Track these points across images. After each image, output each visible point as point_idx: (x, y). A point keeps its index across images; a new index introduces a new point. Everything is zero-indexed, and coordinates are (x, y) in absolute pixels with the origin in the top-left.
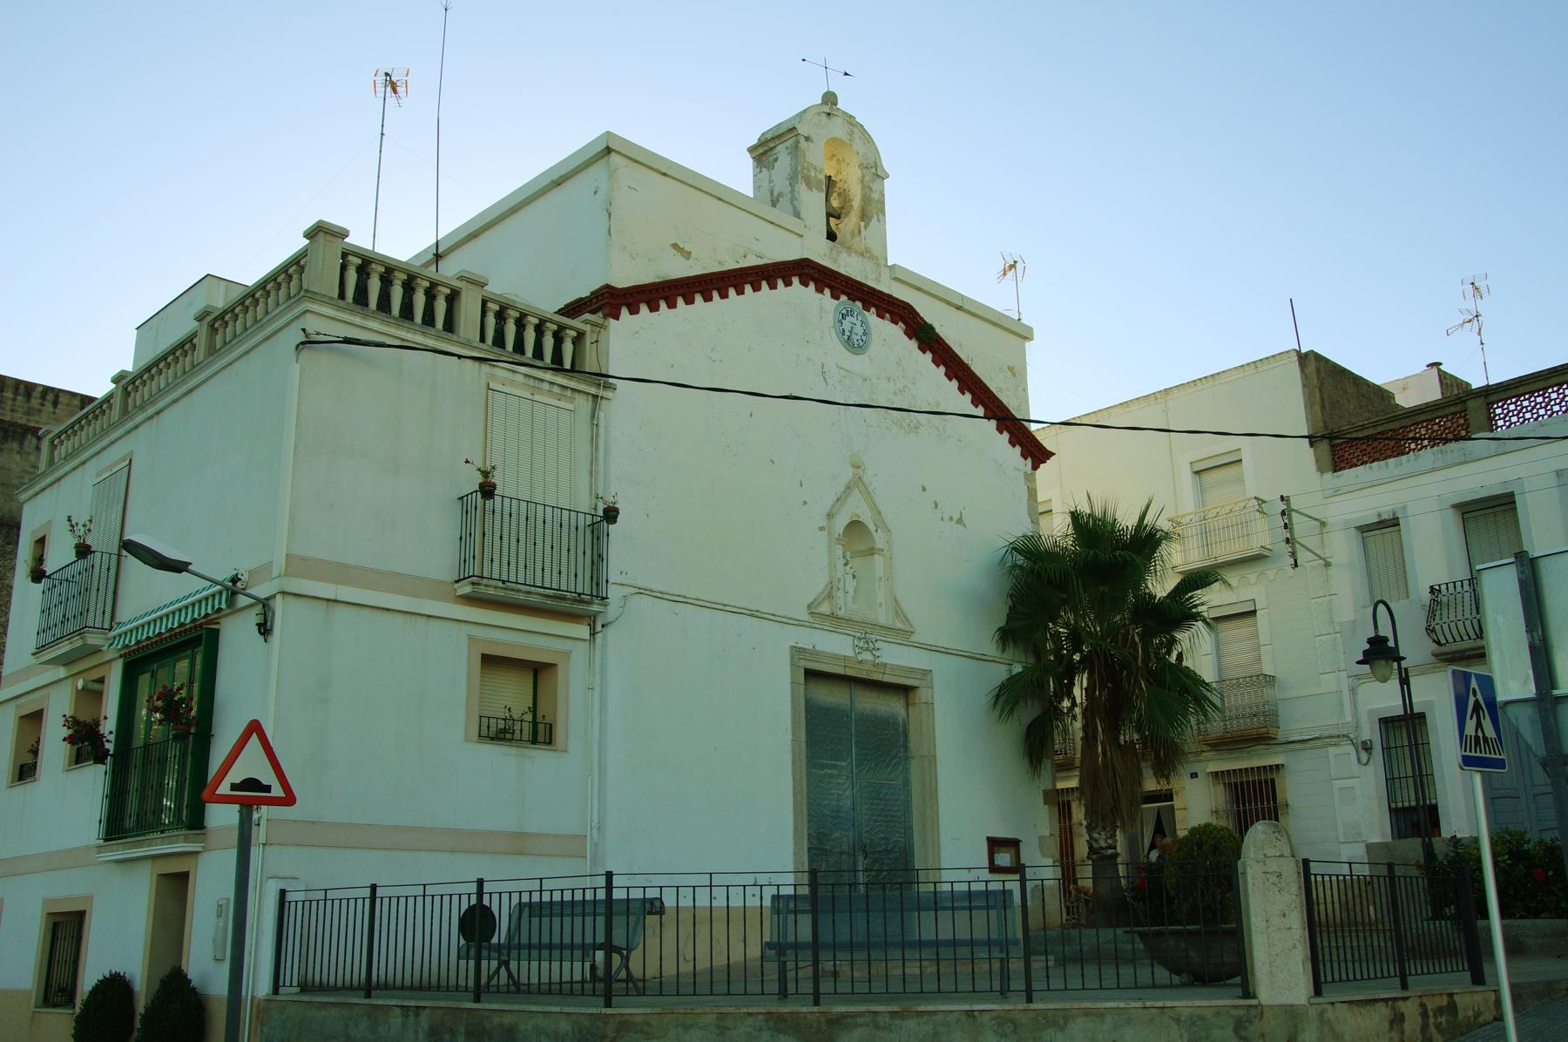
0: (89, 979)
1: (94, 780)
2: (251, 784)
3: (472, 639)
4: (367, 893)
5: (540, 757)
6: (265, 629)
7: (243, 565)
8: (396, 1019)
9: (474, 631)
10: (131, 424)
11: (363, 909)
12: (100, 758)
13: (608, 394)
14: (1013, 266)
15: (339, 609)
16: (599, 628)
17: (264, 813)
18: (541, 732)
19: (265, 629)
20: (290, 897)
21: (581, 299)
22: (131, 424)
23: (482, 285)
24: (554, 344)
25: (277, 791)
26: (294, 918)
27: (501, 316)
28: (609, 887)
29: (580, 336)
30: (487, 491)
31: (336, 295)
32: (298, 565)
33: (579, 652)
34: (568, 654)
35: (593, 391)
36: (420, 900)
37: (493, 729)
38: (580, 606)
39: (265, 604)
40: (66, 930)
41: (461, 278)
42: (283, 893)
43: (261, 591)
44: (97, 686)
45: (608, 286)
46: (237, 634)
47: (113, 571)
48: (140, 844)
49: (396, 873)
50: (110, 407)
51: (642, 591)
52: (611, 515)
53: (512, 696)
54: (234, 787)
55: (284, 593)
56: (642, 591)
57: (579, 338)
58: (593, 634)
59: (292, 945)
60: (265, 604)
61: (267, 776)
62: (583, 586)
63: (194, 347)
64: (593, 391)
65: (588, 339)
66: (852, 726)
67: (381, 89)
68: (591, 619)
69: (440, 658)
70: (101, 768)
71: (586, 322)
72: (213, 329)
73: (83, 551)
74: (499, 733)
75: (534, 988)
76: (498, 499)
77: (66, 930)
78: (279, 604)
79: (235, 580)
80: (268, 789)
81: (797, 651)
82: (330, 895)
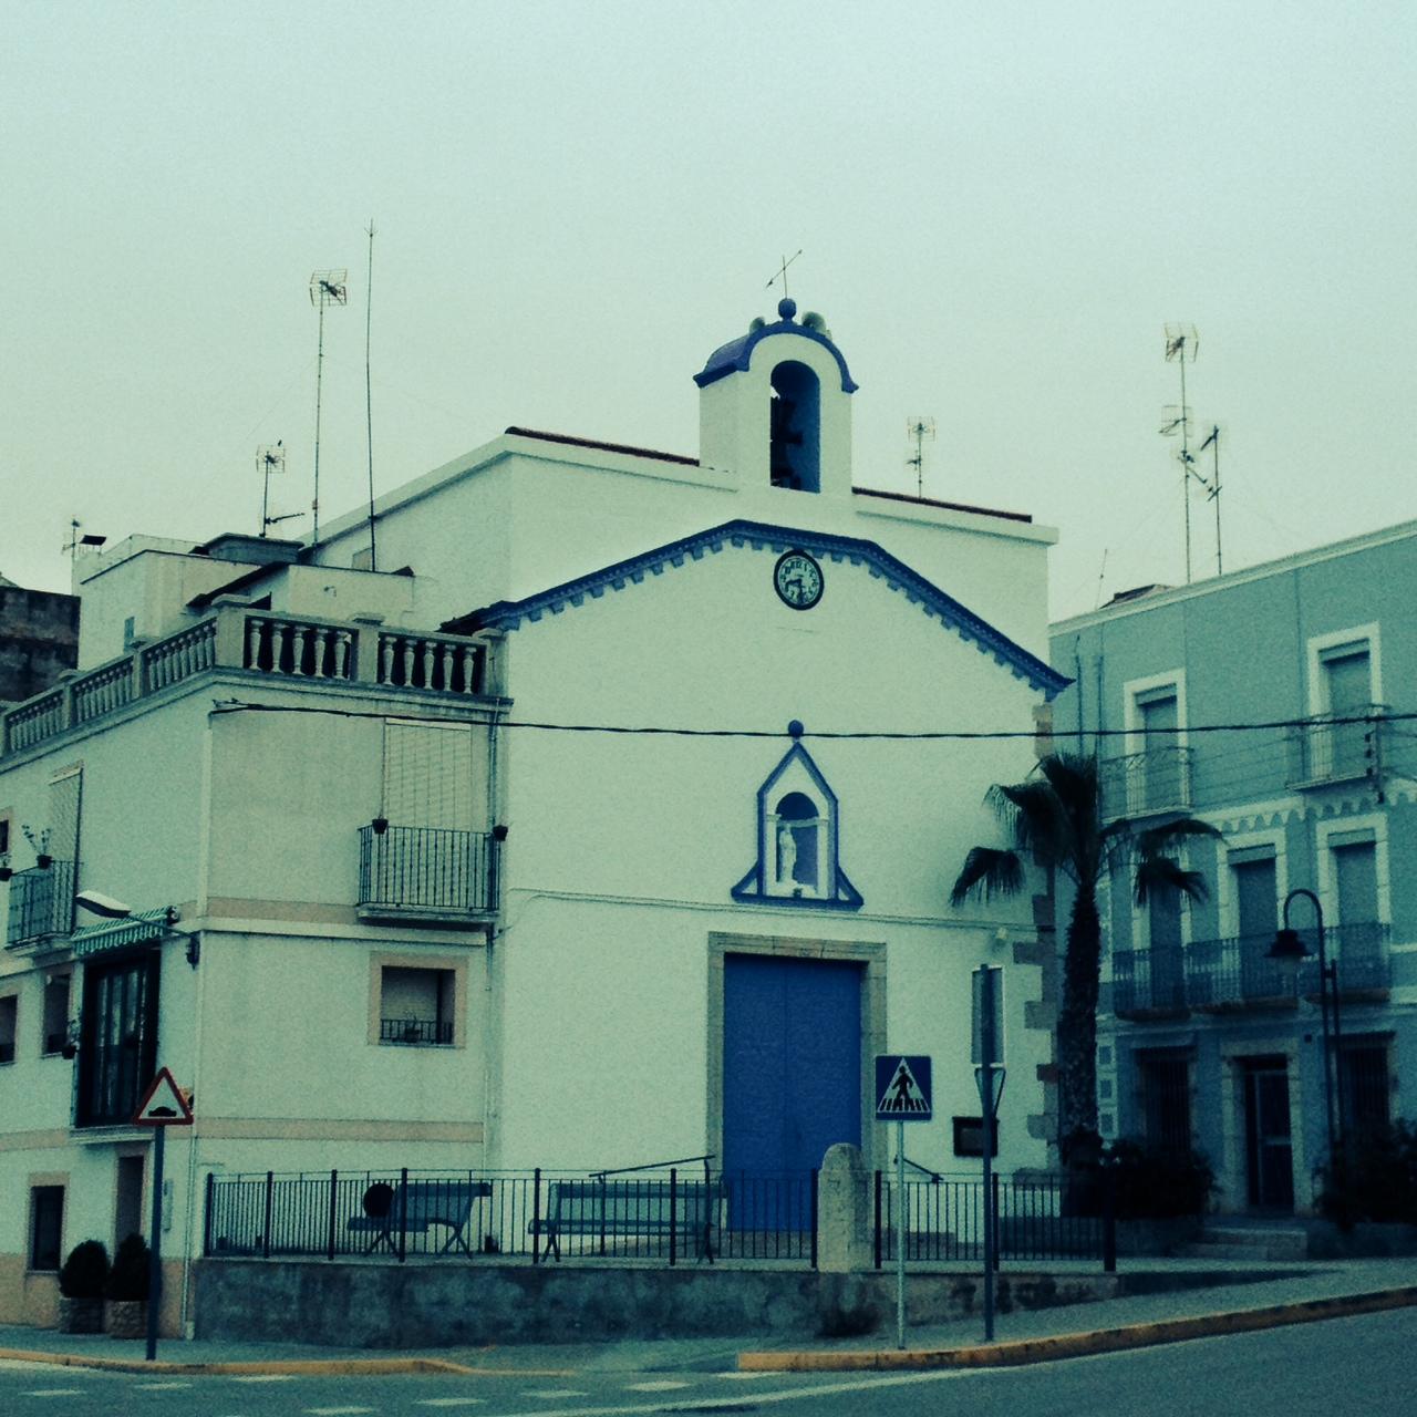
0: (70, 1244)
1: (63, 1073)
2: (163, 1111)
3: (373, 953)
4: (329, 1177)
5: (436, 1057)
6: (193, 958)
7: (175, 899)
8: (281, 1273)
9: (376, 947)
10: (79, 736)
11: (263, 1192)
12: (68, 1054)
13: (508, 708)
14: (1180, 343)
15: (255, 942)
16: (496, 934)
17: (170, 1130)
18: (443, 1034)
19: (193, 958)
20: (217, 1180)
21: (483, 609)
22: (79, 736)
23: (376, 623)
24: (454, 667)
25: (181, 1115)
26: (221, 1197)
27: (400, 647)
28: (404, 1178)
29: (481, 651)
30: (380, 825)
31: (240, 664)
32: (217, 905)
33: (477, 959)
34: (465, 959)
35: (490, 708)
36: (298, 1184)
37: (395, 1032)
38: (480, 922)
39: (193, 938)
40: (48, 1203)
41: (358, 620)
42: (210, 1177)
43: (186, 926)
44: (62, 981)
45: (502, 601)
46: (173, 959)
47: (71, 879)
48: (104, 1132)
49: (290, 1160)
50: (61, 701)
51: (540, 895)
52: (500, 833)
53: (418, 1007)
54: (151, 1113)
55: (207, 932)
56: (540, 895)
57: (479, 656)
58: (490, 939)
59: (221, 1213)
60: (193, 938)
61: (174, 1105)
62: (481, 901)
63: (131, 669)
64: (490, 708)
65: (488, 655)
66: (790, 1022)
67: (317, 296)
68: (490, 931)
69: (346, 981)
70: (70, 1063)
71: (485, 637)
72: (146, 661)
73: (44, 861)
74: (408, 1036)
75: (340, 1250)
76: (391, 830)
77: (48, 1203)
78: (202, 939)
79: (170, 911)
80: (174, 1113)
81: (717, 937)
82: (242, 1180)
